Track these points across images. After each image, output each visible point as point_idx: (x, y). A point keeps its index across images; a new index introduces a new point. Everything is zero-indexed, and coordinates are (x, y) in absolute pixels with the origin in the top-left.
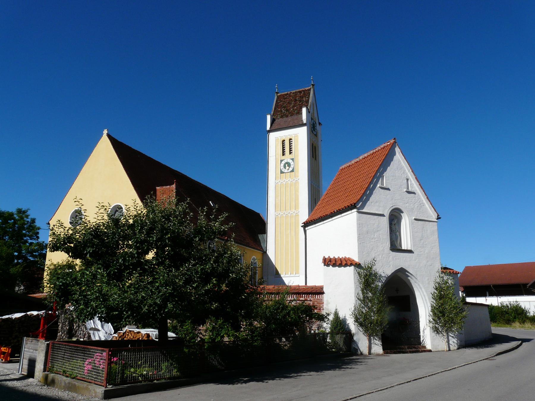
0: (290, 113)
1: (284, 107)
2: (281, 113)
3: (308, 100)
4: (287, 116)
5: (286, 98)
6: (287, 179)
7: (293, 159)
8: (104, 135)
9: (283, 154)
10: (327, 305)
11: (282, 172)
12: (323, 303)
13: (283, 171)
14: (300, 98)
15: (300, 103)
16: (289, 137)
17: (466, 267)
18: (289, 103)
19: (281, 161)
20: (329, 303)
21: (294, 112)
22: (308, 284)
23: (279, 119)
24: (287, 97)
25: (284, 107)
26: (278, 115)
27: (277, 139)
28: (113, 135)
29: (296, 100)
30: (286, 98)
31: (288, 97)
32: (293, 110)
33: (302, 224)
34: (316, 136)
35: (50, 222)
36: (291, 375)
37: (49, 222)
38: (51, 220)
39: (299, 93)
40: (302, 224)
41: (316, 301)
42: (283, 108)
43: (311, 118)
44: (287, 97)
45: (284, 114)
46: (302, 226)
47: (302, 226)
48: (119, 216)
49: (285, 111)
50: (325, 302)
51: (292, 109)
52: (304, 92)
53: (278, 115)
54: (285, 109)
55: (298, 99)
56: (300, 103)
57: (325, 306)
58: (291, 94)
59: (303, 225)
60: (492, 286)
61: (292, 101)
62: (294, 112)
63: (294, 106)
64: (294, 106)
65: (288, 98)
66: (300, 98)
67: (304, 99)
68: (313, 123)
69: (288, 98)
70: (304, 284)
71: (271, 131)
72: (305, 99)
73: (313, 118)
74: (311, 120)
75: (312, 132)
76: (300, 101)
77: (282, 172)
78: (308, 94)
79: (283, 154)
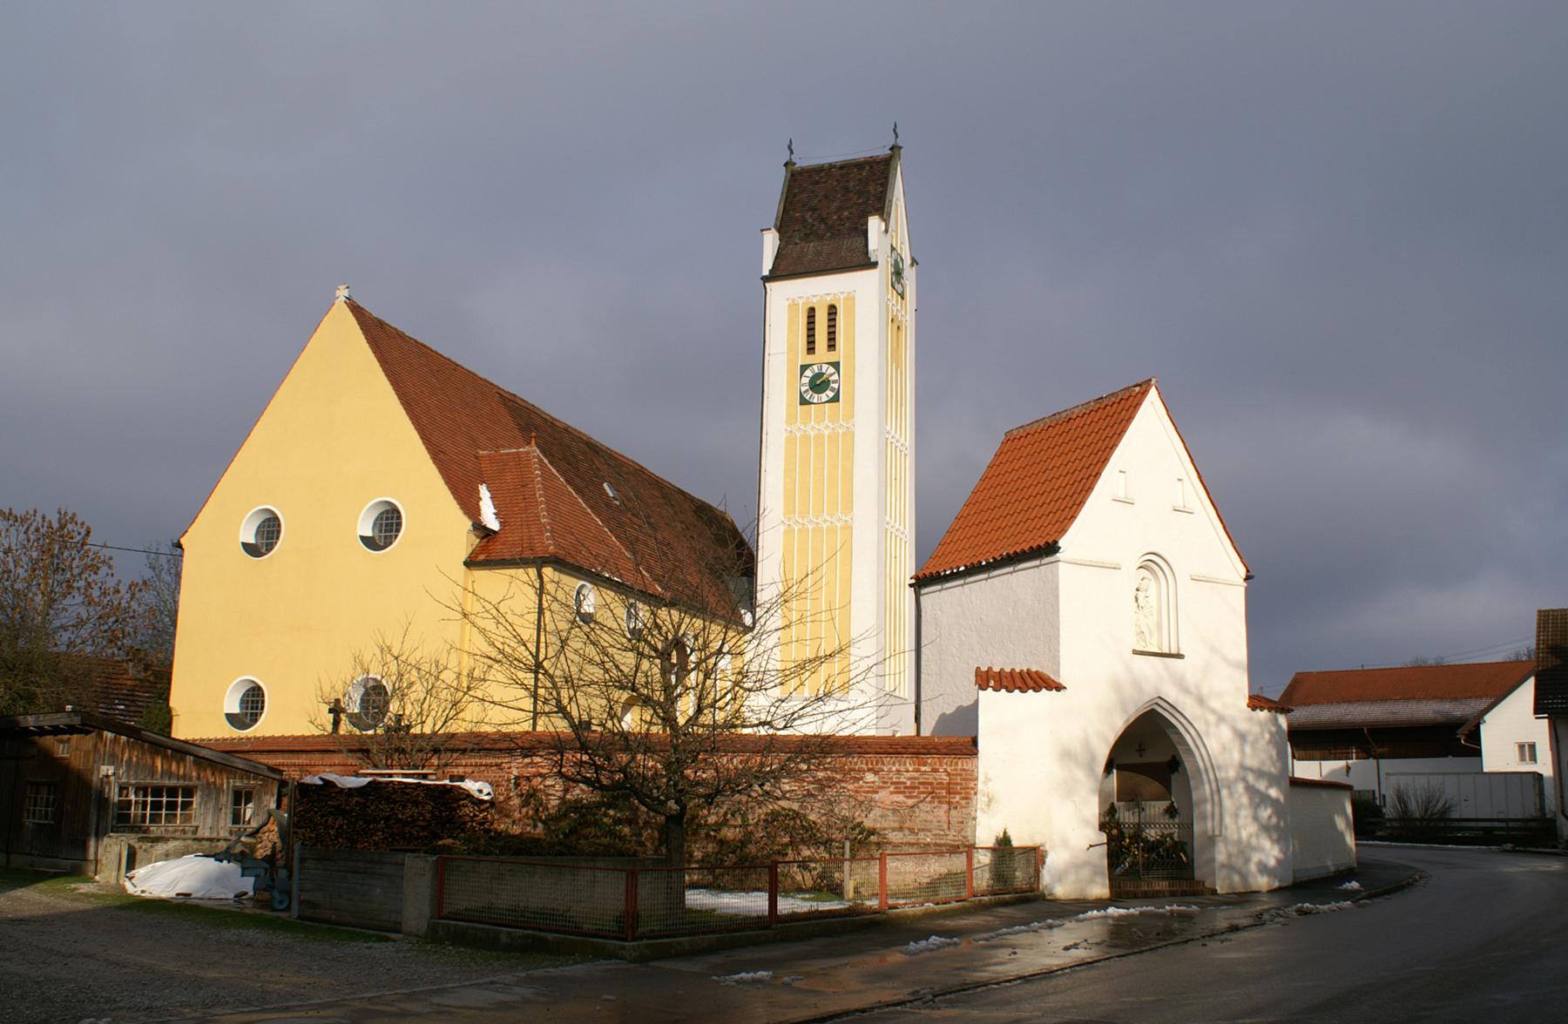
0: (832, 227)
1: (814, 209)
2: (804, 227)
3: (881, 192)
4: (821, 238)
5: (818, 183)
6: (821, 417)
7: (836, 365)
8: (337, 301)
9: (811, 349)
10: (988, 780)
11: (804, 402)
12: (977, 779)
13: (807, 398)
14: (857, 185)
15: (858, 199)
16: (829, 300)
17: (1297, 674)
18: (826, 197)
19: (804, 368)
20: (990, 780)
21: (843, 225)
22: (922, 734)
23: (796, 244)
24: (821, 178)
25: (814, 209)
26: (794, 231)
27: (793, 306)
28: (375, 310)
29: (846, 190)
30: (818, 183)
31: (823, 180)
32: (839, 218)
33: (911, 578)
34: (903, 298)
35: (183, 541)
36: (337, 1020)
37: (179, 541)
38: (186, 534)
39: (855, 170)
40: (911, 578)
41: (961, 775)
42: (807, 211)
43: (892, 246)
44: (821, 178)
45: (811, 229)
46: (911, 585)
47: (911, 585)
48: (567, 589)
49: (814, 220)
50: (981, 778)
51: (835, 217)
52: (871, 167)
53: (796, 233)
54: (816, 215)
55: (854, 186)
56: (860, 201)
57: (980, 786)
58: (833, 170)
59: (913, 581)
60: (1368, 730)
61: (836, 192)
62: (843, 225)
63: (840, 209)
64: (840, 209)
65: (825, 182)
66: (857, 185)
67: (871, 189)
68: (896, 261)
69: (825, 182)
70: (913, 732)
71: (775, 275)
72: (875, 190)
73: (894, 246)
74: (892, 251)
75: (893, 286)
76: (860, 193)
77: (804, 402)
78: (883, 173)
79: (811, 349)
